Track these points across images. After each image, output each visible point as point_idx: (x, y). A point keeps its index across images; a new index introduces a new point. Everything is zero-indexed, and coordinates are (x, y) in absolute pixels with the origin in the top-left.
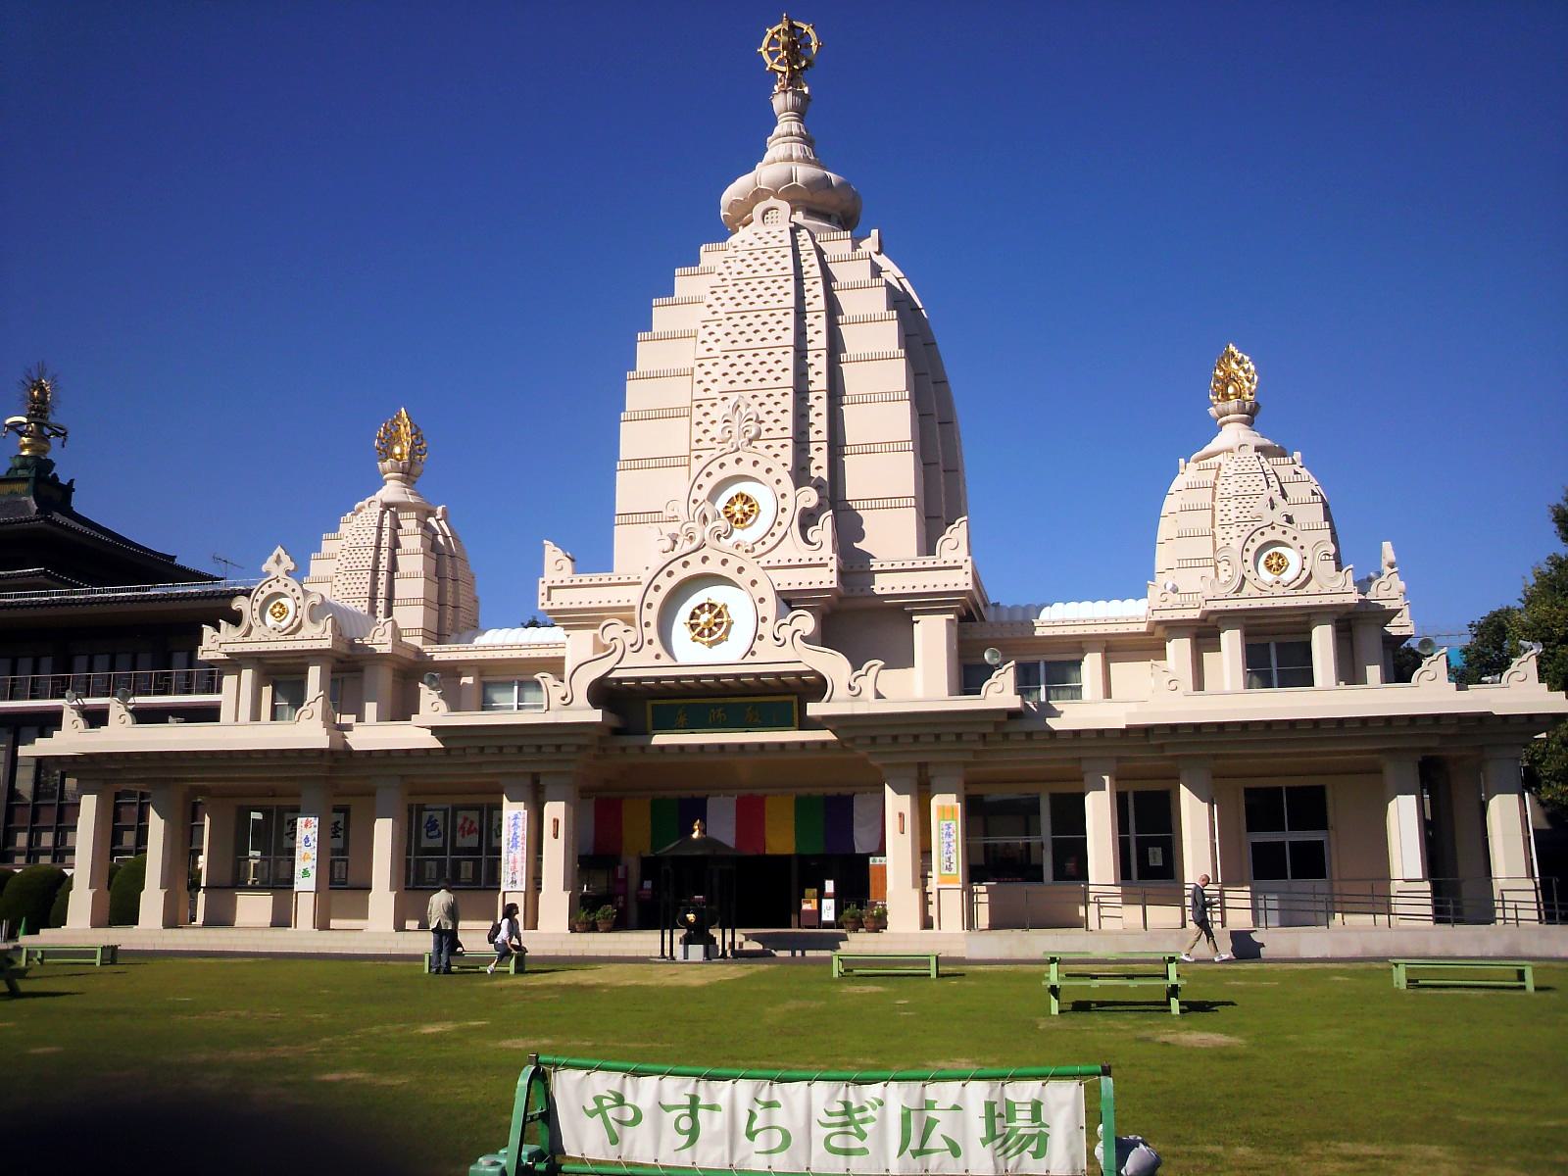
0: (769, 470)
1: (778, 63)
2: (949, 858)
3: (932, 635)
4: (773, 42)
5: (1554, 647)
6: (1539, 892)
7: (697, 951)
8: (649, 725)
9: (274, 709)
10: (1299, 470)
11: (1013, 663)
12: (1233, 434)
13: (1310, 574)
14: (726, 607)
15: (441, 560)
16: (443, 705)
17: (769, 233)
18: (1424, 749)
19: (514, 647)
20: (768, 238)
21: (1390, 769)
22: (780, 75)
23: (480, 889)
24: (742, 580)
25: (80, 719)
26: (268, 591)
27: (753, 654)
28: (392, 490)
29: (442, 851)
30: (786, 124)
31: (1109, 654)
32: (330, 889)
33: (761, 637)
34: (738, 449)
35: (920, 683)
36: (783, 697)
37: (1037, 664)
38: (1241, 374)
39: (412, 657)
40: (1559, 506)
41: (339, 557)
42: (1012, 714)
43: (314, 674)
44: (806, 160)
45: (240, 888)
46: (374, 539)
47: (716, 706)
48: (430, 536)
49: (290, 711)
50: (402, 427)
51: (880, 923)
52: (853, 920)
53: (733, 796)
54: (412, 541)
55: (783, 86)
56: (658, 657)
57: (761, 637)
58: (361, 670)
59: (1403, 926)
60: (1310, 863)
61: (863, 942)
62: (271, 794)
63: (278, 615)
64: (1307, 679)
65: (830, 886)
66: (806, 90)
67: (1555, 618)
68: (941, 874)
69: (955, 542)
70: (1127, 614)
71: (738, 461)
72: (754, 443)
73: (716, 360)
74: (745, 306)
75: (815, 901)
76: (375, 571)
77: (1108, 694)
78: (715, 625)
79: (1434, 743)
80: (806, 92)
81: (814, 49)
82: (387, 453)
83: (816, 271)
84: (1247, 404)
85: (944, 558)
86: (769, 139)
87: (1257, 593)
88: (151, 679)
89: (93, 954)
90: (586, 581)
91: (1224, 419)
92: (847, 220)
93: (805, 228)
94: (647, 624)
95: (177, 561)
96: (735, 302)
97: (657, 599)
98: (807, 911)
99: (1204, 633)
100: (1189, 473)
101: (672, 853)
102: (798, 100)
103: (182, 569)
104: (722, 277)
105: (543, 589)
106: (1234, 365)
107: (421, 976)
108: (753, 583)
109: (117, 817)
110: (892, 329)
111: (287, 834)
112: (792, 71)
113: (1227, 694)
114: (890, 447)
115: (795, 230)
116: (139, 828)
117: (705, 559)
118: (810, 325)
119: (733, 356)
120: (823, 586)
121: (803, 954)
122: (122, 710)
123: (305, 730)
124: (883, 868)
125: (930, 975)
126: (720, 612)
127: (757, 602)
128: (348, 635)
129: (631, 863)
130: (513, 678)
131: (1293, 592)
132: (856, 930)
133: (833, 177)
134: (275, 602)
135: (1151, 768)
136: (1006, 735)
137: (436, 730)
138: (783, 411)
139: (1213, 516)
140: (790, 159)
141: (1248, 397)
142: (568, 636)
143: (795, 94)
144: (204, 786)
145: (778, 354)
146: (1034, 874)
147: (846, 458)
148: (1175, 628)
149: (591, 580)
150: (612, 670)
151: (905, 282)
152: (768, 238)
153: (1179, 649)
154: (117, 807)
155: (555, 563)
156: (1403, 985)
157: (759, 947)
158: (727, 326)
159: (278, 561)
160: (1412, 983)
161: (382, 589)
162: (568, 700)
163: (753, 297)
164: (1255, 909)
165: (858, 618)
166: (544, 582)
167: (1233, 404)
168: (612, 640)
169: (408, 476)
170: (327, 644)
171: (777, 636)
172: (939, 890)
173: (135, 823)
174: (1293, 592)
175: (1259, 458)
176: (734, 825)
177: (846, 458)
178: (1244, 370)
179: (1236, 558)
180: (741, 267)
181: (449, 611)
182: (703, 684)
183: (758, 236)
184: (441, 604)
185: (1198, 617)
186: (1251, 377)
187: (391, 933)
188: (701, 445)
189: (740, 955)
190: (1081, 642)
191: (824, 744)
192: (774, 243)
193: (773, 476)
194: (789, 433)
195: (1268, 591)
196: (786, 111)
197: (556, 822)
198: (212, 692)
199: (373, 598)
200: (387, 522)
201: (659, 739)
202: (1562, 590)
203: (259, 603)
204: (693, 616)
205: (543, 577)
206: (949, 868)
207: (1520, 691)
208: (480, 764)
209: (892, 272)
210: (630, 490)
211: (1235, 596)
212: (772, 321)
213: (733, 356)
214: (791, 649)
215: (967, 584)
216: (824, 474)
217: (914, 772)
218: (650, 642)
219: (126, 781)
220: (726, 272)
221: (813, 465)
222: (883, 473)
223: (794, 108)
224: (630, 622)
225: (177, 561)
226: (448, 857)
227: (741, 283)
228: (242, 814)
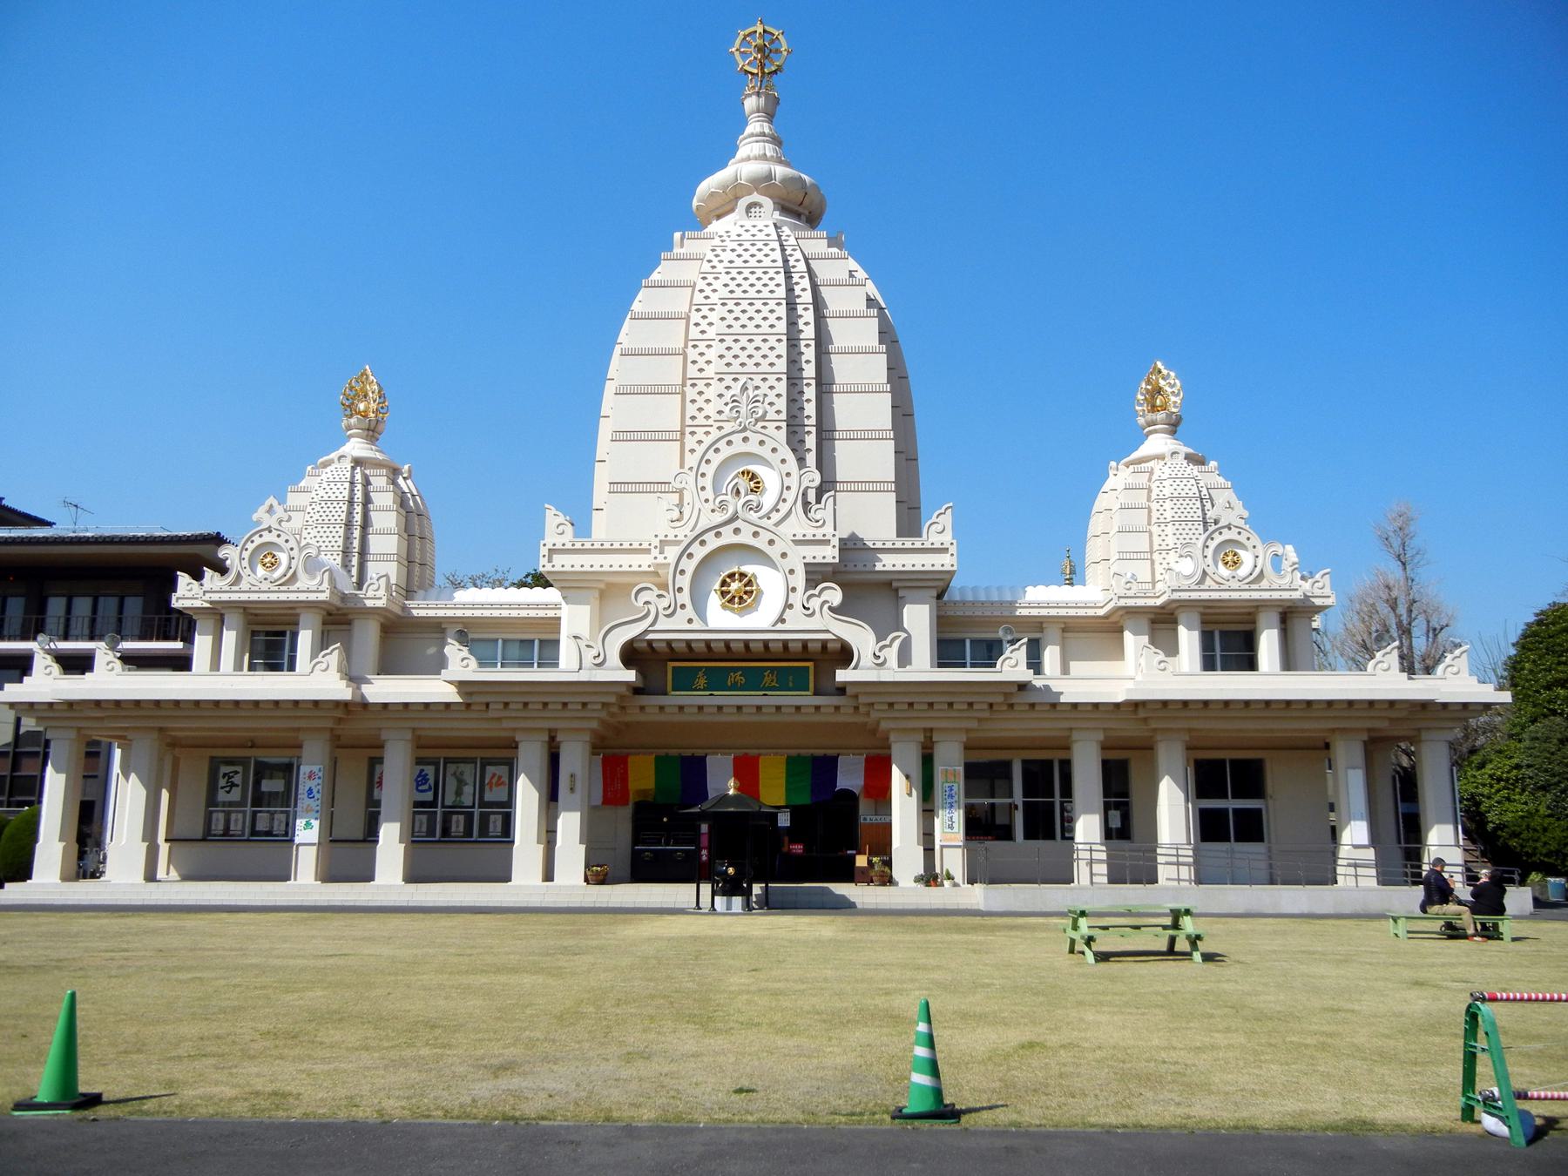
13: (1266, 570)
15: (412, 519)
16: (473, 663)
18: (1369, 730)
30: (755, 126)
33: (791, 607)
34: (745, 429)
37: (963, 641)
41: (309, 509)
47: (735, 669)
54: (383, 499)
57: (791, 607)
58: (349, 623)
60: (1250, 828)
64: (1250, 664)
69: (939, 528)
70: (1092, 595)
72: (760, 424)
74: (739, 293)
79: (1384, 724)
90: (908, 545)
97: (689, 566)
100: (1119, 477)
105: (544, 551)
110: (873, 325)
113: (1179, 674)
119: (729, 340)
122: (111, 656)
123: (315, 676)
135: (1130, 743)
136: (1011, 706)
137: (462, 686)
146: (1006, 833)
155: (556, 528)
159: (270, 510)
167: (1161, 416)
170: (323, 597)
178: (1171, 384)
179: (1198, 553)
180: (733, 256)
181: (417, 568)
188: (723, 417)
192: (761, 236)
194: (783, 416)
195: (1229, 585)
200: (358, 477)
204: (724, 583)
206: (951, 827)
208: (499, 719)
210: (612, 461)
212: (765, 310)
213: (729, 340)
214: (818, 617)
218: (683, 606)
219: (95, 734)
220: (715, 261)
222: (867, 458)
224: (664, 586)
226: (439, 810)
227: (734, 272)
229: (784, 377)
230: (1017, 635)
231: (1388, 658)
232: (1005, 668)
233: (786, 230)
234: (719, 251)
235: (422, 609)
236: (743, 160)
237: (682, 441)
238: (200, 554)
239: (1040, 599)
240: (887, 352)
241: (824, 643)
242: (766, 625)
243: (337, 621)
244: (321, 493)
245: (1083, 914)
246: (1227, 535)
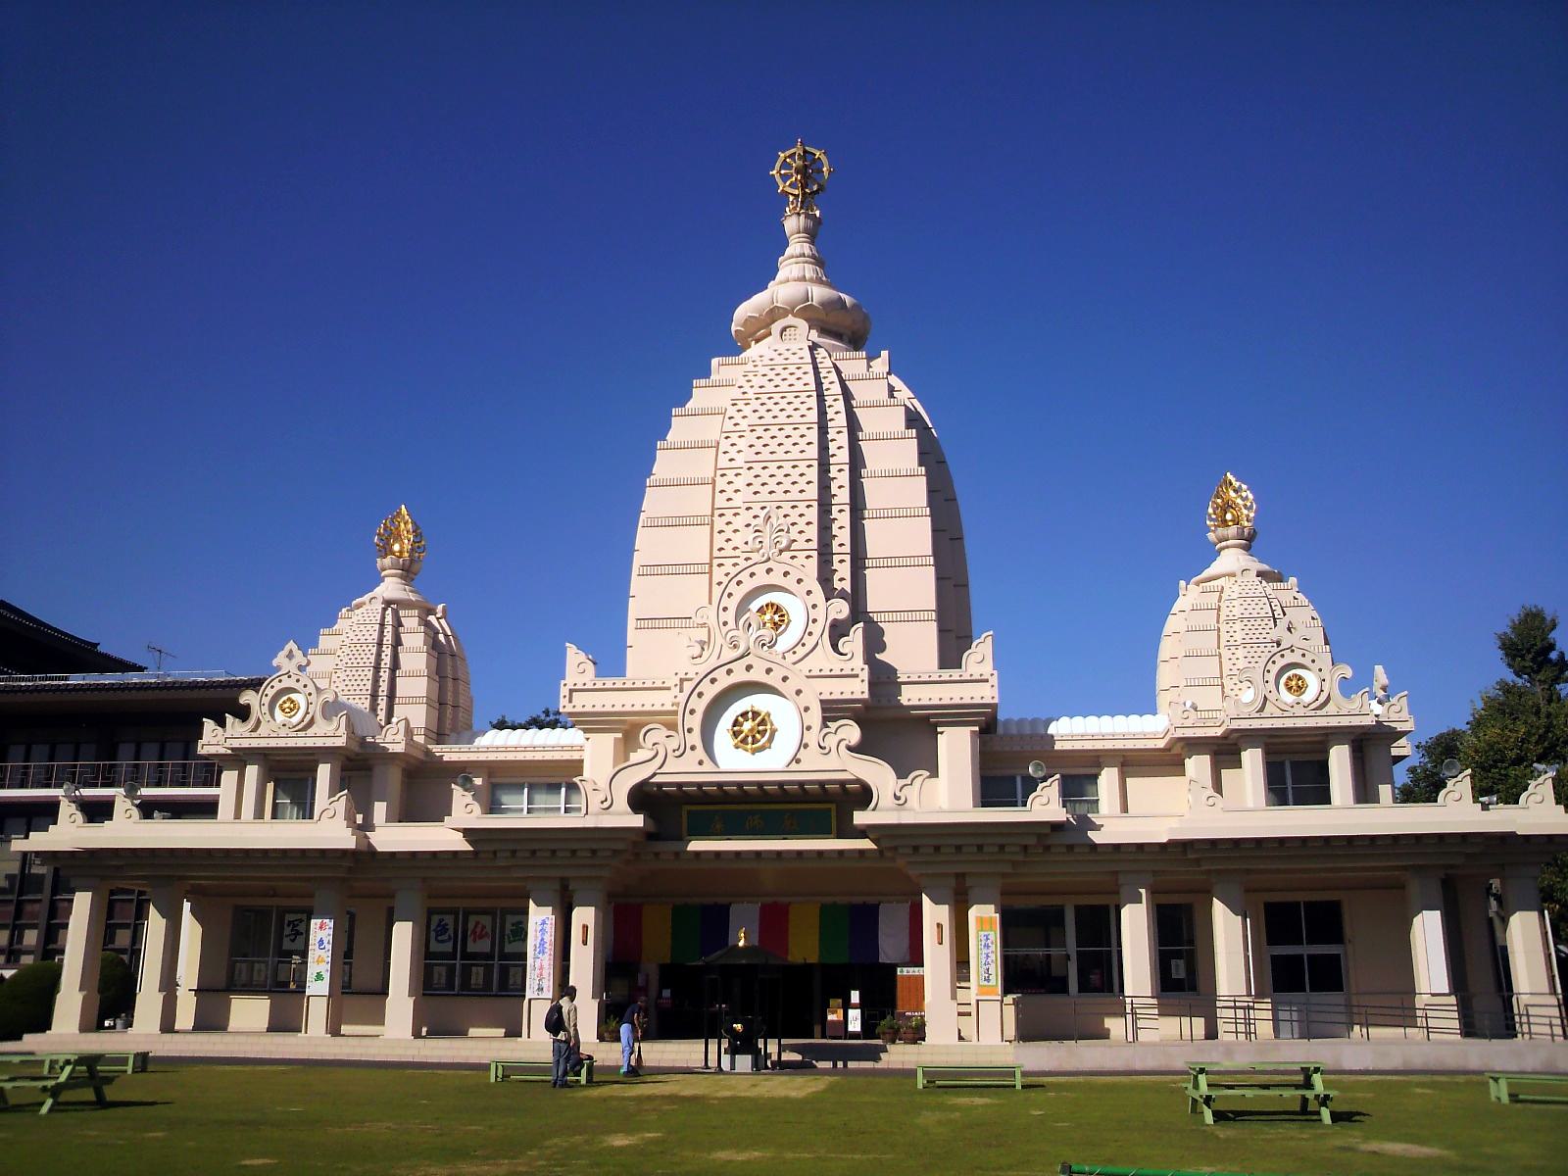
0: (799, 581)
1: (790, 185)
2: (988, 970)
3: (955, 747)
4: (785, 165)
5: (1506, 768)
6: (1563, 1008)
7: (744, 1062)
8: (685, 832)
9: (275, 806)
10: (1297, 595)
11: (1058, 776)
12: (1231, 558)
13: (1323, 695)
14: (769, 715)
15: (441, 657)
16: (477, 808)
17: (788, 350)
19: (518, 749)
20: (787, 354)
21: (1414, 887)
22: (791, 198)
23: (490, 996)
24: (788, 688)
25: (79, 813)
26: (278, 686)
27: (798, 761)
28: (390, 587)
29: (489, 956)
30: (797, 246)
31: (1125, 769)
32: (343, 993)
33: (806, 746)
35: (944, 793)
36: (830, 805)
37: (1013, 779)
38: (1239, 501)
39: (421, 756)
40: (1505, 633)
41: (339, 653)
42: (1056, 827)
43: (324, 772)
44: (819, 281)
45: (235, 991)
46: (376, 635)
48: (432, 634)
49: (292, 809)
50: (402, 525)
51: (918, 1034)
52: (891, 1031)
53: (757, 903)
54: (414, 640)
55: (795, 208)
56: (701, 763)
58: (370, 769)
59: (1433, 1035)
60: (1328, 976)
61: (663, 1052)
62: (271, 892)
63: (288, 710)
64: (1323, 797)
65: (855, 997)
66: (818, 213)
67: (1507, 741)
68: (979, 986)
69: (980, 658)
70: (1147, 729)
71: (769, 571)
73: (738, 471)
74: (768, 419)
75: (841, 1012)
76: (377, 668)
77: (1125, 809)
78: (759, 732)
80: (818, 215)
81: (826, 174)
82: (386, 551)
83: (836, 389)
84: (1246, 531)
85: (970, 672)
86: (781, 259)
87: (1279, 713)
88: (53, 770)
89: (124, 1061)
90: (609, 685)
91: (1224, 544)
92: (855, 340)
93: (821, 347)
94: (690, 730)
95: (99, 648)
96: (758, 414)
97: (700, 705)
98: (833, 1021)
99: (1225, 751)
100: (1189, 596)
101: (723, 961)
102: (810, 223)
103: (106, 656)
104: (742, 390)
105: (564, 691)
106: (1232, 494)
107: (489, 1085)
108: (799, 692)
109: (110, 915)
110: (911, 447)
111: (287, 936)
112: (804, 194)
113: (1242, 808)
114: (891, 563)
115: (813, 347)
116: (136, 926)
117: (749, 668)
118: (832, 440)
120: (854, 697)
121: (845, 1065)
123: (327, 828)
124: (920, 981)
125: (1014, 1086)
126: (763, 719)
127: (802, 711)
128: (359, 732)
129: (650, 970)
130: (521, 780)
131: (1313, 713)
132: (894, 1042)
133: (848, 299)
134: (285, 698)
135: (1184, 877)
136: (1047, 848)
137: (469, 833)
138: (808, 523)
139: (1219, 636)
140: (803, 279)
141: (1246, 524)
142: (588, 739)
143: (807, 216)
144: (200, 885)
145: (802, 467)
146: (1060, 986)
147: (867, 572)
148: (1194, 745)
149: (624, 683)
150: (654, 775)
151: (916, 402)
152: (787, 354)
153: (1198, 766)
154: (111, 904)
155: (577, 666)
156: (1505, 1099)
157: (799, 1057)
158: (751, 438)
159: (290, 656)
160: (1514, 1097)
161: (384, 687)
162: (606, 805)
163: (776, 410)
164: (1276, 1020)
165: (892, 727)
166: (565, 685)
167: (1233, 530)
168: (654, 745)
169: (408, 573)
170: (341, 742)
171: (822, 745)
172: (978, 1001)
173: (131, 921)
174: (1313, 713)
175: (1261, 583)
176: (908, 931)
177: (867, 572)
178: (1243, 498)
181: (449, 710)
182: (685, 792)
183: (778, 352)
184: (442, 704)
185: (1219, 734)
186: (1249, 504)
187: (74, 1034)
188: (723, 553)
189: (781, 1066)
190: (1098, 757)
191: (862, 852)
192: (794, 359)
193: (805, 587)
194: (814, 545)
195: (1290, 711)
196: (799, 233)
197: (585, 928)
198: (211, 786)
199: (374, 696)
201: (696, 845)
202: (1511, 714)
203: (269, 698)
204: (736, 723)
205: (564, 679)
206: (988, 980)
207: (1535, 812)
208: (508, 868)
209: (904, 393)
210: (644, 596)
211: (1258, 715)
213: (758, 468)
214: (835, 757)
215: (993, 698)
216: (847, 586)
217: (952, 882)
219: (129, 884)
221: (836, 577)
222: (905, 589)
223: (806, 231)
224: (672, 726)
225: (99, 648)
226: (496, 963)
228: (256, 917)
229: (815, 504)
230: (1052, 772)
231: (1459, 787)
232: (1036, 806)
233: (821, 353)
234: (751, 376)
235: (451, 753)
236: (781, 283)
237: (710, 573)
238: (225, 703)
239: (1104, 730)
240: (928, 474)
241: (842, 783)
242: (781, 766)
243: (359, 768)
244: (351, 635)
245: (1202, 1071)
246: (1290, 658)
